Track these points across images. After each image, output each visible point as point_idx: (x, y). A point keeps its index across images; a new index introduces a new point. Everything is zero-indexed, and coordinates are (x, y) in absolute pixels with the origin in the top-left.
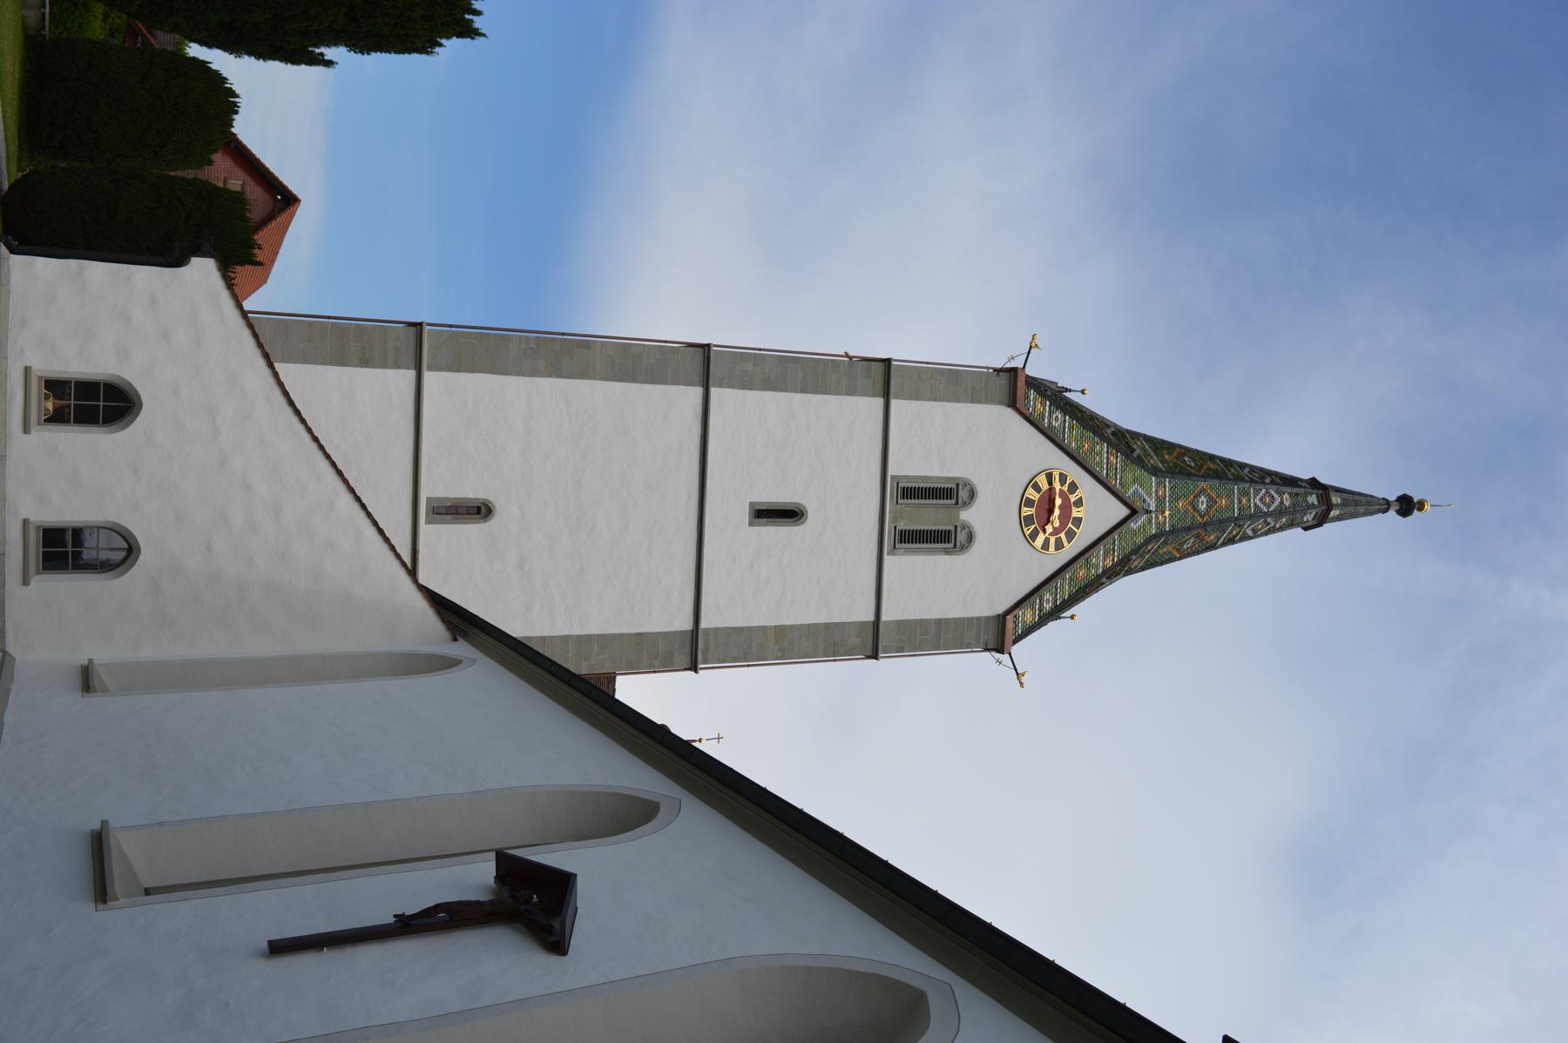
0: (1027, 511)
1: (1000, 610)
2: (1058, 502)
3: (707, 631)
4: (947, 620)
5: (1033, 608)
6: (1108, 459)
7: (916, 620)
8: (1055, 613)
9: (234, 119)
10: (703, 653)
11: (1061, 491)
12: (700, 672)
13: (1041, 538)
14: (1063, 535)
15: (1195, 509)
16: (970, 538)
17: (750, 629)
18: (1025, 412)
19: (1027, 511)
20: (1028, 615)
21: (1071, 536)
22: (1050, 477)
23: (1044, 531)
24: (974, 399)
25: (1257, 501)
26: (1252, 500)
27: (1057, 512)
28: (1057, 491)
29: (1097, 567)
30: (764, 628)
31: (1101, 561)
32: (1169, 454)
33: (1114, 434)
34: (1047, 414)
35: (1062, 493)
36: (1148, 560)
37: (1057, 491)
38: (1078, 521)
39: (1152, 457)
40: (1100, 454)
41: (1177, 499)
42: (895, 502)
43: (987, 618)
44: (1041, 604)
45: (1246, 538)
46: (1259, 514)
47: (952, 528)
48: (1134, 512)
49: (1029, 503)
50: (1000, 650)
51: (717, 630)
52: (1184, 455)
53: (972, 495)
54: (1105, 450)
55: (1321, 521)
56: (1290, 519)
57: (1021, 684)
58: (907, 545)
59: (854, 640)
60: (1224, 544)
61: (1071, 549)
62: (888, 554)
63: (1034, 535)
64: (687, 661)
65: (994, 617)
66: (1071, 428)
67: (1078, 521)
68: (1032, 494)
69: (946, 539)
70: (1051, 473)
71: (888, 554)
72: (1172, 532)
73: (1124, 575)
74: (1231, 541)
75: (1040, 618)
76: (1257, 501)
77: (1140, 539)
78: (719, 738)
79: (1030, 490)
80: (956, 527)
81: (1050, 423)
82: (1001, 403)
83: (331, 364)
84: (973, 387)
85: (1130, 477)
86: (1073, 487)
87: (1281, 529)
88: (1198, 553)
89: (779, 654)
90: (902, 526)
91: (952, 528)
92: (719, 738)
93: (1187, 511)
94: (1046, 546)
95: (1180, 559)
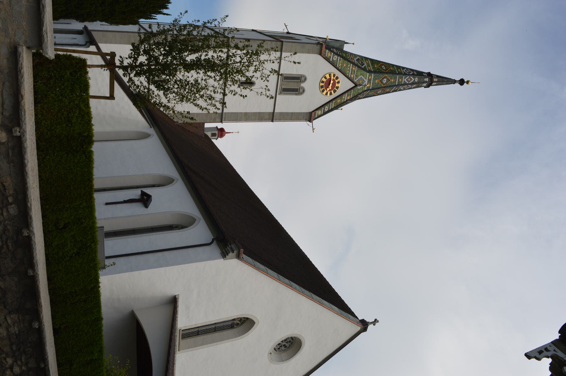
0: (322, 84)
1: (311, 111)
2: (332, 82)
3: (225, 113)
4: (295, 113)
5: (318, 114)
6: (352, 68)
7: (285, 112)
8: (336, 108)
9: (83, 28)
10: (224, 118)
11: (333, 79)
12: (223, 123)
13: (325, 92)
14: (332, 92)
15: (382, 83)
16: (304, 91)
17: (237, 113)
18: (325, 57)
19: (322, 84)
20: (319, 112)
21: (335, 91)
22: (330, 75)
23: (327, 90)
24: (308, 53)
25: (405, 80)
26: (403, 80)
27: (331, 85)
28: (332, 79)
29: (344, 99)
30: (241, 113)
31: (345, 97)
32: (377, 65)
33: (358, 60)
34: (332, 57)
35: (333, 80)
36: (365, 96)
37: (332, 79)
38: (337, 88)
39: (370, 66)
40: (350, 67)
41: (376, 80)
42: (282, 80)
43: (307, 113)
44: (324, 109)
45: (400, 90)
46: (405, 84)
47: (299, 88)
48: (356, 86)
49: (323, 82)
50: (310, 121)
51: (228, 113)
52: (383, 65)
53: (305, 79)
54: (352, 66)
55: (428, 86)
56: (418, 85)
57: (313, 131)
58: (284, 92)
59: (267, 117)
60: (393, 92)
61: (334, 95)
62: (278, 95)
63: (323, 91)
64: (220, 120)
65: (309, 112)
66: (340, 60)
67: (337, 88)
68: (324, 80)
69: (298, 91)
70: (331, 74)
71: (278, 95)
72: (373, 89)
73: (357, 99)
74: (395, 91)
75: (323, 113)
76: (405, 80)
77: (360, 91)
78: (238, 132)
79: (323, 78)
80: (300, 88)
81: (332, 59)
82: (317, 54)
83: (127, 44)
84: (309, 49)
85: (359, 73)
86: (337, 78)
87: (414, 88)
88: (383, 94)
89: (245, 120)
90: (283, 87)
91: (299, 88)
92: (238, 132)
93: (379, 83)
94: (327, 94)
95: (377, 95)
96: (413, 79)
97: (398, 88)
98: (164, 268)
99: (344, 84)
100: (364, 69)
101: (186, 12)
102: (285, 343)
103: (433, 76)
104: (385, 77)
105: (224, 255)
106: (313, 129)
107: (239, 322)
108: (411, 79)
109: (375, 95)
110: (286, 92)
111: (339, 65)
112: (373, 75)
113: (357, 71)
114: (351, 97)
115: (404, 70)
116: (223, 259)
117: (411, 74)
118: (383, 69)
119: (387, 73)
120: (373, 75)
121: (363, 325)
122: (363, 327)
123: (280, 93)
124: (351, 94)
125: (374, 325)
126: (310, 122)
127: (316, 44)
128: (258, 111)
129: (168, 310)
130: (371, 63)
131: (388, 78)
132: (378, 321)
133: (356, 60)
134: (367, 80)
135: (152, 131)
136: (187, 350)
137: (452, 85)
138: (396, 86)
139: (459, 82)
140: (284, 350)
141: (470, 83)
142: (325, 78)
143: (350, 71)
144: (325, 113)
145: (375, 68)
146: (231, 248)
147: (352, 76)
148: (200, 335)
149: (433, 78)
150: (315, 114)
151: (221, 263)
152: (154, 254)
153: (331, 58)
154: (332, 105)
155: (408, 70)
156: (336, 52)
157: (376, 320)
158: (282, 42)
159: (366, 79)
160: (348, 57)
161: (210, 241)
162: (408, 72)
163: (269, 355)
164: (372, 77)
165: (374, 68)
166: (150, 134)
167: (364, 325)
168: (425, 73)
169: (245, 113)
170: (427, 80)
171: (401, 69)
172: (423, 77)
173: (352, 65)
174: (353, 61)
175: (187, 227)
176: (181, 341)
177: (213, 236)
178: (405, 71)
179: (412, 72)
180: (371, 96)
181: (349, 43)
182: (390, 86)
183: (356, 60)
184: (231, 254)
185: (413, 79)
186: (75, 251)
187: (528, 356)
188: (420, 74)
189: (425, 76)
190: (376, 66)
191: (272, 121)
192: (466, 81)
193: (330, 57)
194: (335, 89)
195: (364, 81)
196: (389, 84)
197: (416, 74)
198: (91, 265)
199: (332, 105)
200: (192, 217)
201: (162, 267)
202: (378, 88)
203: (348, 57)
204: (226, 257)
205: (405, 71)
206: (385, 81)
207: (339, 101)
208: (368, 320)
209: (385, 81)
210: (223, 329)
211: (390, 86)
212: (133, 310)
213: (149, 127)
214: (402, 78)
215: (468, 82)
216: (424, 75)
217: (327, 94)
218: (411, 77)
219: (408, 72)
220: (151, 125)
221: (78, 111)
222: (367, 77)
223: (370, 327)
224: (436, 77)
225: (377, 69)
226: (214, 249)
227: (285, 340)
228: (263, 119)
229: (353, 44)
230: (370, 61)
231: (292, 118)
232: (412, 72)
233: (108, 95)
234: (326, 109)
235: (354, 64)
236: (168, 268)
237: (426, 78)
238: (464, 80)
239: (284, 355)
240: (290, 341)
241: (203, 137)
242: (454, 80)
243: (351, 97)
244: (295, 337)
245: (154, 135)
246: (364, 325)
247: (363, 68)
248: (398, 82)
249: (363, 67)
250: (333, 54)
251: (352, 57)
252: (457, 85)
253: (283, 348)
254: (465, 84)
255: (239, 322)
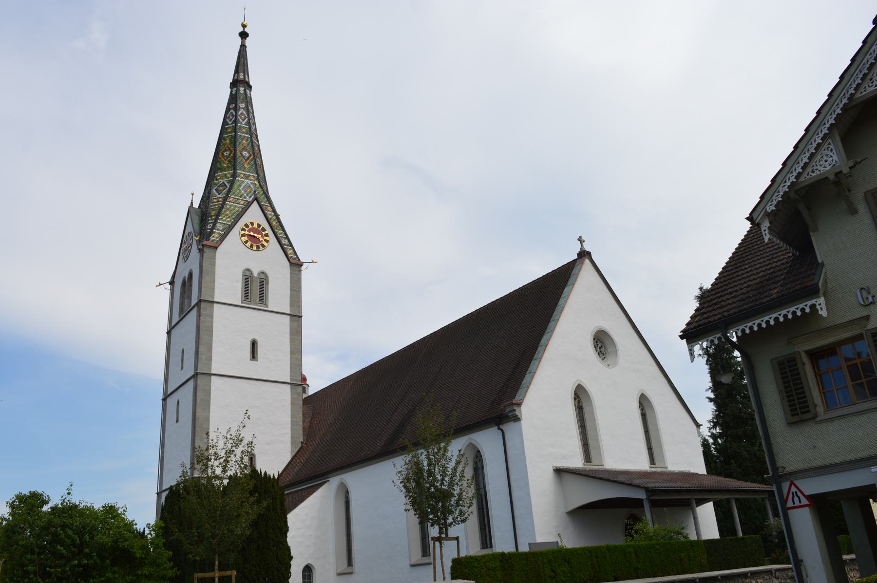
1: (288, 264)
2: (252, 233)
6: (232, 202)
13: (264, 243)
14: (264, 233)
15: (248, 159)
16: (263, 273)
18: (220, 242)
20: (290, 252)
21: (263, 229)
22: (243, 236)
24: (214, 265)
27: (256, 235)
28: (248, 233)
29: (272, 215)
30: (291, 358)
31: (270, 213)
37: (248, 233)
38: (259, 226)
39: (226, 174)
40: (231, 206)
43: (291, 270)
46: (248, 123)
47: (259, 279)
49: (252, 246)
51: (291, 376)
53: (248, 270)
55: (250, 87)
56: (249, 102)
57: (316, 262)
60: (258, 141)
61: (269, 231)
62: (268, 308)
63: (263, 246)
67: (259, 226)
68: (249, 244)
69: (263, 281)
71: (268, 308)
72: (257, 173)
75: (291, 246)
76: (243, 123)
79: (247, 245)
81: (222, 231)
82: (215, 253)
84: (210, 264)
90: (258, 301)
91: (259, 279)
94: (267, 241)
95: (263, 164)
96: (242, 110)
97: (254, 134)
98: (529, 482)
99: (254, 215)
100: (232, 183)
101: (393, 481)
102: (599, 348)
103: (236, 78)
104: (241, 154)
105: (517, 419)
106: (313, 262)
107: (577, 400)
108: (242, 113)
109: (263, 167)
110: (264, 297)
111: (229, 221)
112: (239, 171)
113: (235, 195)
114: (269, 205)
115: (230, 123)
116: (522, 421)
117: (234, 113)
118: (230, 155)
119: (235, 150)
120: (239, 171)
121: (585, 256)
122: (586, 257)
123: (266, 305)
124: (265, 205)
125: (584, 242)
126: (302, 265)
127: (203, 254)
128: (288, 336)
129: (567, 477)
130: (220, 172)
131: (242, 149)
132: (580, 237)
133: (219, 194)
134: (245, 183)
135: (334, 482)
136: (602, 456)
137: (249, 50)
138: (251, 137)
139: (243, 39)
140: (605, 348)
141: (245, 23)
142: (246, 242)
143: (235, 206)
144: (291, 245)
145: (228, 167)
146: (510, 412)
147: (242, 202)
148: (587, 443)
149: (239, 79)
150: (293, 258)
151: (525, 423)
152: (512, 490)
153: (221, 232)
154: (280, 234)
155: (229, 117)
156: (212, 225)
157: (579, 240)
158: (200, 301)
159: (244, 182)
160: (217, 206)
161: (500, 431)
162: (231, 117)
163: (610, 367)
164: (241, 172)
165: (228, 168)
166: (339, 483)
167: (584, 254)
168: (231, 92)
169: (291, 354)
170: (242, 89)
171: (227, 128)
172: (238, 95)
173: (228, 201)
174: (221, 199)
175: (479, 451)
176: (594, 463)
177: (494, 426)
178: (230, 121)
179: (232, 110)
180: (264, 174)
181: (192, 201)
182: (252, 146)
183: (219, 194)
184: (517, 413)
185: (242, 110)
186: (567, 564)
187: (692, 361)
188: (233, 99)
189: (236, 90)
190: (225, 166)
191: (301, 317)
192: (241, 29)
193: (219, 234)
194: (261, 229)
195: (247, 186)
196: (249, 147)
197: (234, 105)
198: (575, 553)
199: (280, 232)
200: (467, 446)
201: (528, 483)
202: (256, 164)
203: (217, 206)
204: (520, 418)
205: (230, 121)
206: (246, 153)
207: (274, 223)
208: (578, 250)
209: (245, 154)
210: (583, 418)
211: (252, 146)
212: (567, 513)
213: (328, 483)
214: (241, 127)
215: (244, 26)
216: (236, 93)
217: (267, 241)
218: (240, 113)
219: (231, 117)
220: (325, 480)
221: (488, 563)
222: (241, 181)
223: (587, 248)
224: (237, 75)
225: (230, 163)
226: (509, 428)
227: (595, 348)
228: (299, 329)
229: (193, 194)
230: (217, 173)
231: (297, 289)
232: (232, 110)
233: (456, 541)
234: (285, 241)
235: (225, 199)
236: (530, 478)
237: (239, 90)
238: (241, 32)
239: (610, 349)
240: (597, 342)
241: (313, 407)
242: (240, 46)
243: (269, 205)
244: (594, 336)
245: (342, 478)
246: (584, 254)
247: (230, 186)
248: (247, 134)
249: (228, 186)
250: (215, 229)
251: (215, 200)
252: (248, 42)
253: (603, 350)
254: (246, 30)
255: (577, 400)
